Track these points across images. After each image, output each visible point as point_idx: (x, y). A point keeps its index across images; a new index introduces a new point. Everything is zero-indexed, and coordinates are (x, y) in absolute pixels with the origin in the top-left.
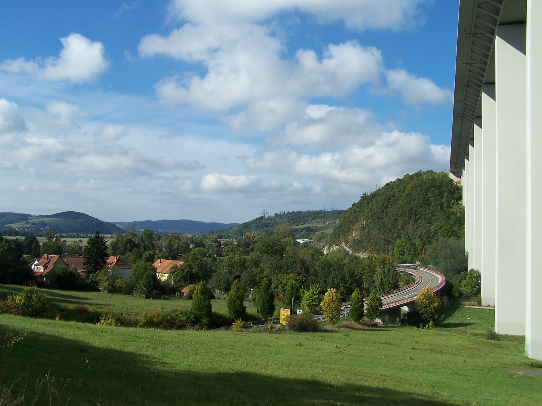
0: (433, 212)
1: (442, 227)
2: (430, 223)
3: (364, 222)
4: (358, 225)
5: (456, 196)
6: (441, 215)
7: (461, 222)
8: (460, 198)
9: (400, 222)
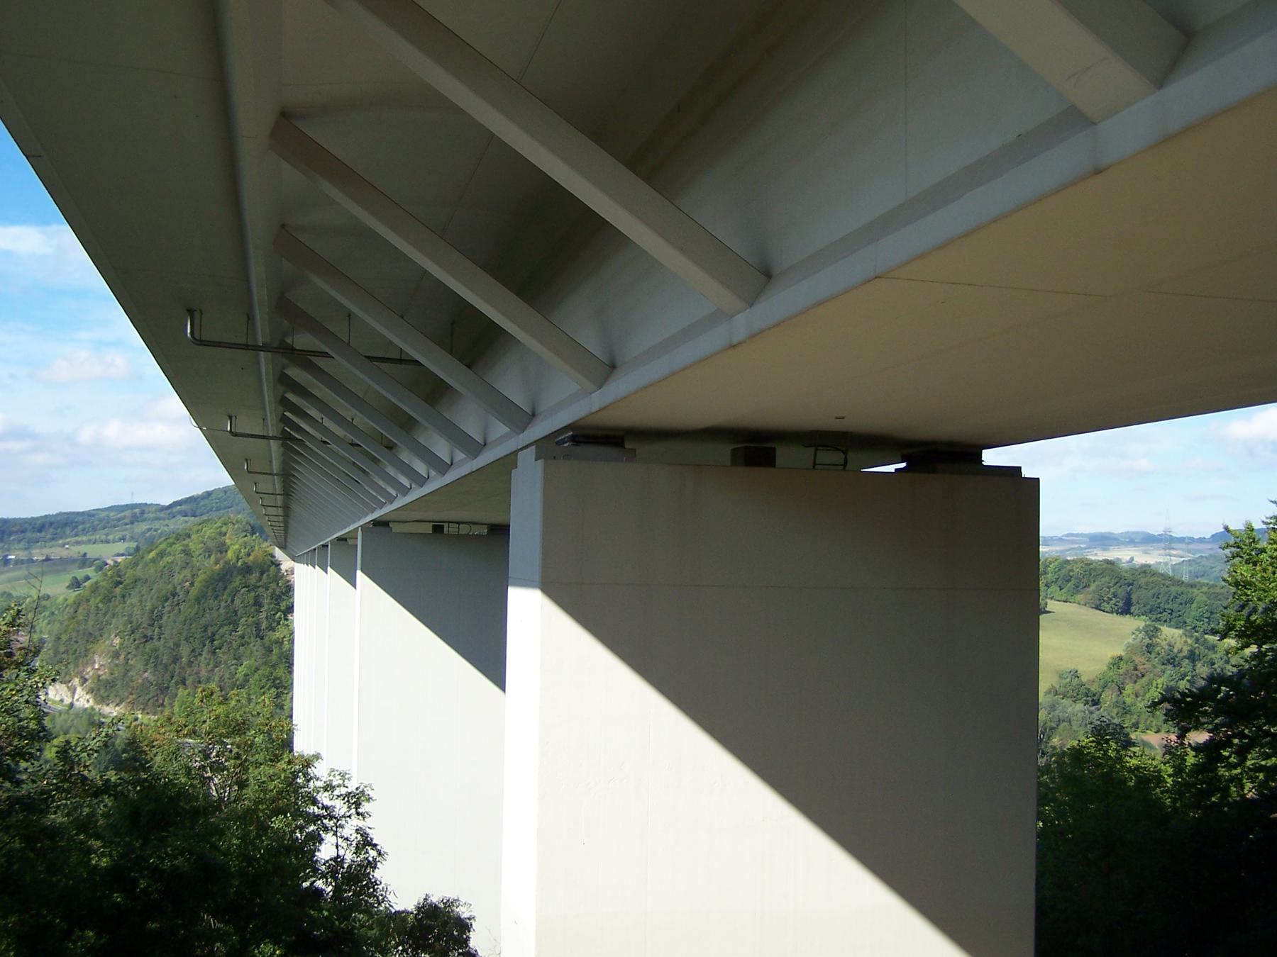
0: (242, 637)
1: (257, 669)
2: (238, 659)
3: (117, 641)
4: (102, 646)
5: (283, 605)
6: (256, 647)
7: (287, 660)
8: (290, 609)
9: (185, 651)
